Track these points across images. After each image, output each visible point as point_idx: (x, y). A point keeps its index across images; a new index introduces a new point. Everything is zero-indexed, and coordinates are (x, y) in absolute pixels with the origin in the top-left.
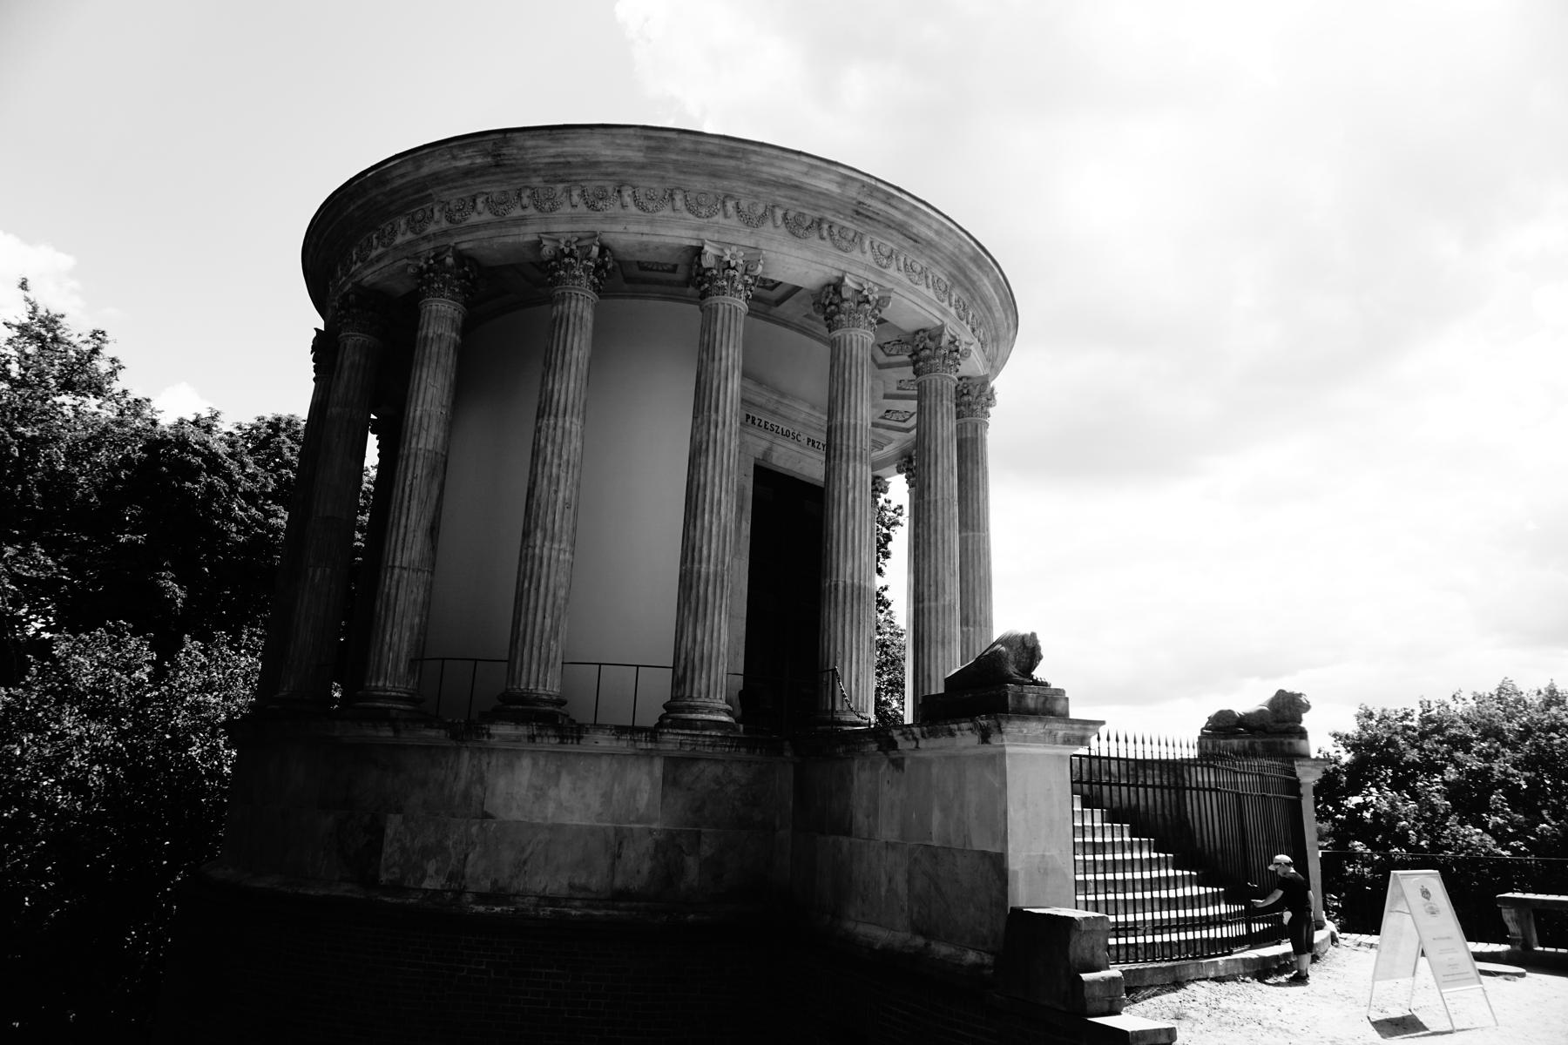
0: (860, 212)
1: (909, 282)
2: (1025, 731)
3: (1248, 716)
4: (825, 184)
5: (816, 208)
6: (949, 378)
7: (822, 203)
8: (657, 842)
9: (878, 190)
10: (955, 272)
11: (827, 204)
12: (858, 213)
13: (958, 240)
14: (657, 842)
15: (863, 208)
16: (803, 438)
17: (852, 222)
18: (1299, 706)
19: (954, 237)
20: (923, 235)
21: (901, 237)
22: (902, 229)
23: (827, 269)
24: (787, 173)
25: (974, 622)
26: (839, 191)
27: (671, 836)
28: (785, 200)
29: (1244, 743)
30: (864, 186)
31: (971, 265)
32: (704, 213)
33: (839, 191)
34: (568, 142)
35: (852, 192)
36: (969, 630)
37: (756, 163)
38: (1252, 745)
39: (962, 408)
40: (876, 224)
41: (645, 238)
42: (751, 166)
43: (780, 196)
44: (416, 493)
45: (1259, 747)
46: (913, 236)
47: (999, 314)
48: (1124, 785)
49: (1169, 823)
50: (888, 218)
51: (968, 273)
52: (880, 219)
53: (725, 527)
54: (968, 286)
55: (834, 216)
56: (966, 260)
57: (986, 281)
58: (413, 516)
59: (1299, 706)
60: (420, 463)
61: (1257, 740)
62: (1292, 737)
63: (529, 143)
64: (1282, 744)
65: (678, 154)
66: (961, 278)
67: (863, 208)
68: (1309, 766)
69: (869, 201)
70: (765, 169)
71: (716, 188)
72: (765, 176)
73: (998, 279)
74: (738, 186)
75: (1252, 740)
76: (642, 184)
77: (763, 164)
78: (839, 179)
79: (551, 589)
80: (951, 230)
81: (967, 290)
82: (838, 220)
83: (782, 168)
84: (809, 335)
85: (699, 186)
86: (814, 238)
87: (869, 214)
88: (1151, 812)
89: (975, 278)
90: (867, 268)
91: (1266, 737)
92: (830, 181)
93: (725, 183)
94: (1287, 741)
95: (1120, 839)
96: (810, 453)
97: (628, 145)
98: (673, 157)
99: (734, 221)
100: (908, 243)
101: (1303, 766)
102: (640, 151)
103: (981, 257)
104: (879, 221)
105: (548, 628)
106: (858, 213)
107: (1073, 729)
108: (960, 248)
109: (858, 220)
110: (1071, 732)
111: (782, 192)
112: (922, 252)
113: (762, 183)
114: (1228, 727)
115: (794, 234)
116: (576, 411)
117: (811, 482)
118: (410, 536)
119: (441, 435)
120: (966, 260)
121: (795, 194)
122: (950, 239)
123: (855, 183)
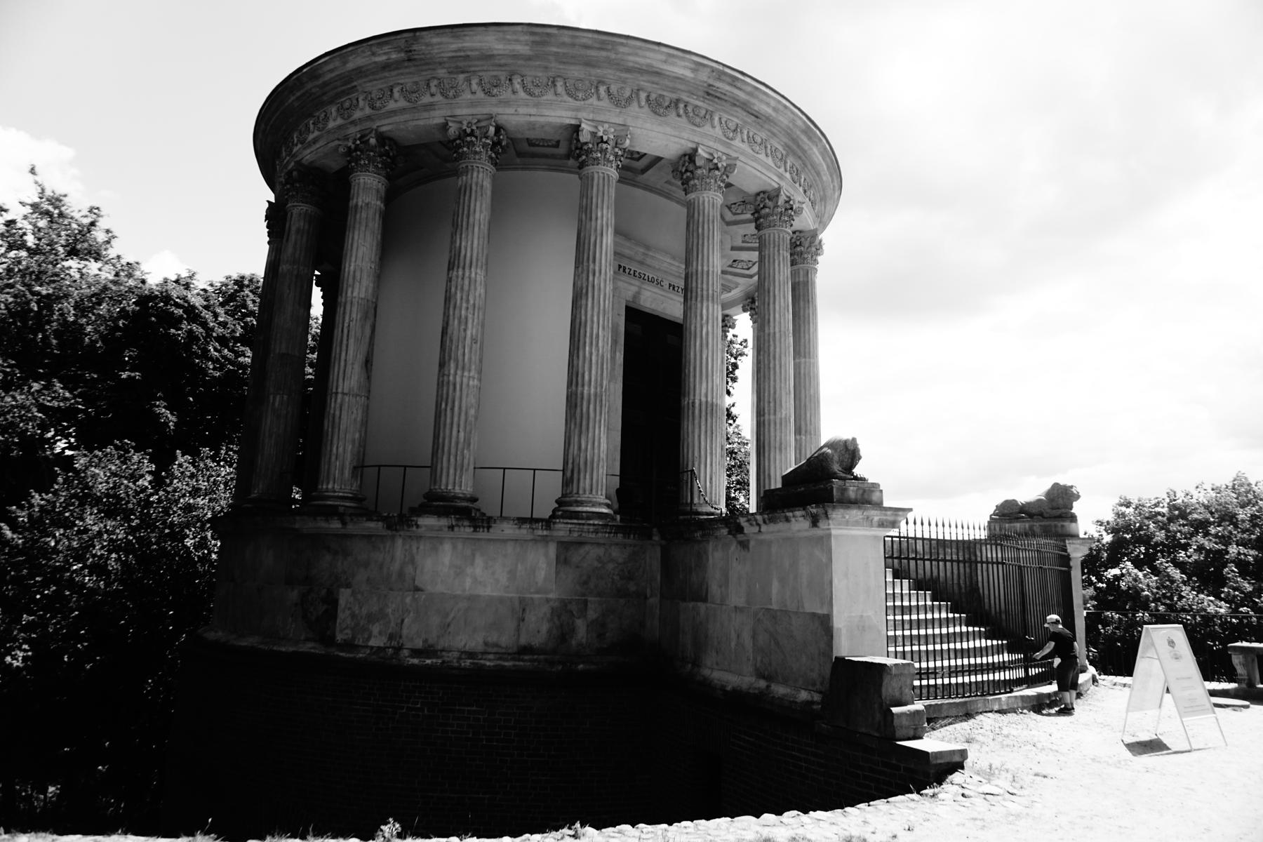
1: (751, 152)
2: (847, 517)
3: (1029, 504)
5: (674, 90)
6: (785, 231)
7: (680, 86)
9: (725, 74)
10: (790, 143)
12: (708, 94)
16: (666, 284)
17: (704, 102)
19: (789, 113)
20: (762, 112)
21: (745, 114)
22: (745, 107)
25: (806, 432)
27: (564, 604)
30: (713, 71)
31: (803, 137)
34: (467, 38)
35: (704, 76)
37: (623, 53)
38: (1031, 528)
39: (796, 257)
41: (533, 119)
42: (619, 56)
43: (643, 81)
44: (352, 333)
45: (1037, 530)
46: (754, 113)
47: (826, 177)
48: (928, 560)
49: (963, 590)
50: (734, 98)
52: (726, 98)
53: (603, 356)
54: (801, 154)
55: (688, 97)
56: (798, 133)
57: (815, 150)
58: (351, 352)
60: (355, 309)
62: (1064, 521)
63: (435, 40)
64: (1056, 526)
65: (558, 47)
66: (795, 147)
69: (718, 84)
70: (631, 58)
71: (590, 76)
72: (631, 64)
73: (825, 148)
74: (609, 73)
75: (1032, 523)
77: (629, 54)
79: (464, 409)
80: (786, 107)
81: (800, 158)
83: (645, 57)
85: (576, 74)
88: (950, 582)
90: (717, 140)
92: (685, 67)
93: (599, 71)
94: (1060, 524)
95: (923, 603)
97: (517, 41)
98: (555, 49)
99: (605, 103)
100: (750, 119)
102: (527, 45)
103: (812, 130)
104: (726, 101)
105: (462, 440)
106: (708, 94)
107: (886, 515)
108: (793, 121)
109: (709, 100)
110: (885, 518)
111: (646, 78)
112: (762, 126)
113: (628, 70)
115: (655, 113)
116: (479, 264)
117: (672, 319)
118: (349, 368)
119: (371, 285)
120: (798, 133)
121: (656, 79)
123: (706, 69)
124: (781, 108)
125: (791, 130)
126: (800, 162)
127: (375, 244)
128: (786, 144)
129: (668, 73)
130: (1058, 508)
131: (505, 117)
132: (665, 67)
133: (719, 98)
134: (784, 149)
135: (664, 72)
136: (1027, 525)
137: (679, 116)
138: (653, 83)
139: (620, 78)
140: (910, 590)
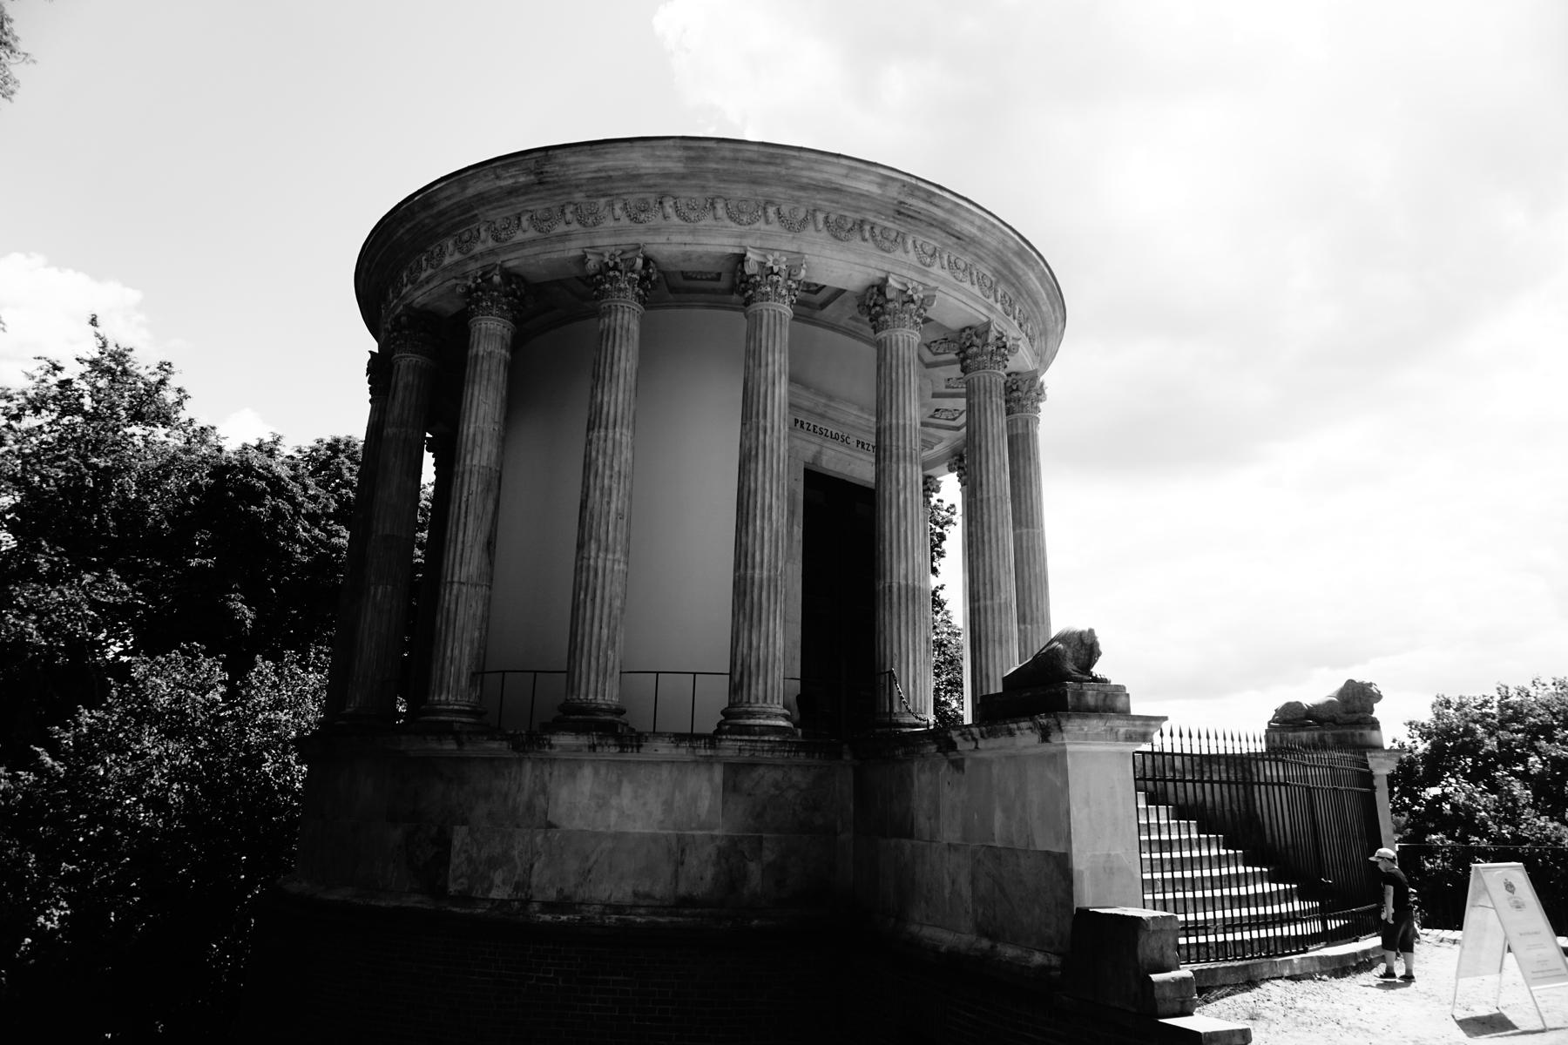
0: (901, 212)
3: (1316, 707)
4: (866, 185)
5: (857, 210)
6: (998, 374)
8: (719, 848)
9: (919, 188)
10: (1000, 268)
11: (868, 206)
12: (900, 213)
13: (1003, 236)
14: (719, 848)
15: (904, 208)
16: (853, 441)
17: (894, 222)
18: (1370, 697)
19: (998, 233)
21: (944, 235)
22: (944, 227)
23: (870, 270)
24: (826, 176)
25: (1032, 620)
26: (879, 192)
27: (733, 842)
28: (827, 203)
29: (1313, 735)
30: (904, 186)
32: (745, 220)
33: (879, 192)
34: (608, 156)
35: (893, 192)
36: (1026, 628)
38: (1321, 738)
40: (918, 223)
41: (688, 248)
42: (791, 171)
43: (820, 200)
45: (1329, 740)
47: (1046, 307)
50: (930, 217)
51: (1013, 267)
53: (777, 532)
54: (1014, 281)
55: (875, 217)
56: (1010, 255)
57: (1031, 275)
58: (470, 532)
59: (1370, 697)
60: (474, 480)
61: (1326, 732)
62: (1362, 728)
63: (571, 159)
65: (717, 163)
66: (1005, 272)
67: (904, 208)
68: (1383, 757)
69: (910, 201)
71: (756, 195)
72: (805, 180)
73: (1044, 273)
74: (779, 192)
75: (1322, 732)
76: (683, 194)
77: (802, 169)
78: (879, 180)
80: (994, 225)
81: (1013, 285)
82: (880, 221)
84: (854, 337)
85: (739, 193)
86: (856, 240)
87: (910, 213)
88: (1209, 804)
89: (1020, 273)
90: (910, 267)
91: (1335, 729)
92: (871, 182)
94: (1358, 732)
96: (861, 456)
97: (667, 157)
99: (776, 227)
100: (952, 241)
101: (1376, 757)
102: (680, 161)
104: (921, 220)
105: (605, 638)
106: (900, 213)
107: (1135, 726)
108: (1004, 242)
110: (1133, 729)
111: (823, 195)
114: (1295, 720)
116: (625, 422)
117: (862, 484)
118: (467, 550)
119: (495, 451)
120: (1010, 255)
121: (835, 197)
122: (994, 234)
123: (895, 183)
124: (987, 225)
125: (1001, 252)
126: (1014, 290)
127: (499, 400)
128: (995, 269)
129: (850, 190)
130: (1355, 712)
131: (655, 247)
132: (846, 182)
133: (912, 217)
134: (994, 275)
135: (844, 189)
136: (1316, 734)
137: (864, 240)
138: (833, 202)
139: (793, 197)
140: (1168, 820)
